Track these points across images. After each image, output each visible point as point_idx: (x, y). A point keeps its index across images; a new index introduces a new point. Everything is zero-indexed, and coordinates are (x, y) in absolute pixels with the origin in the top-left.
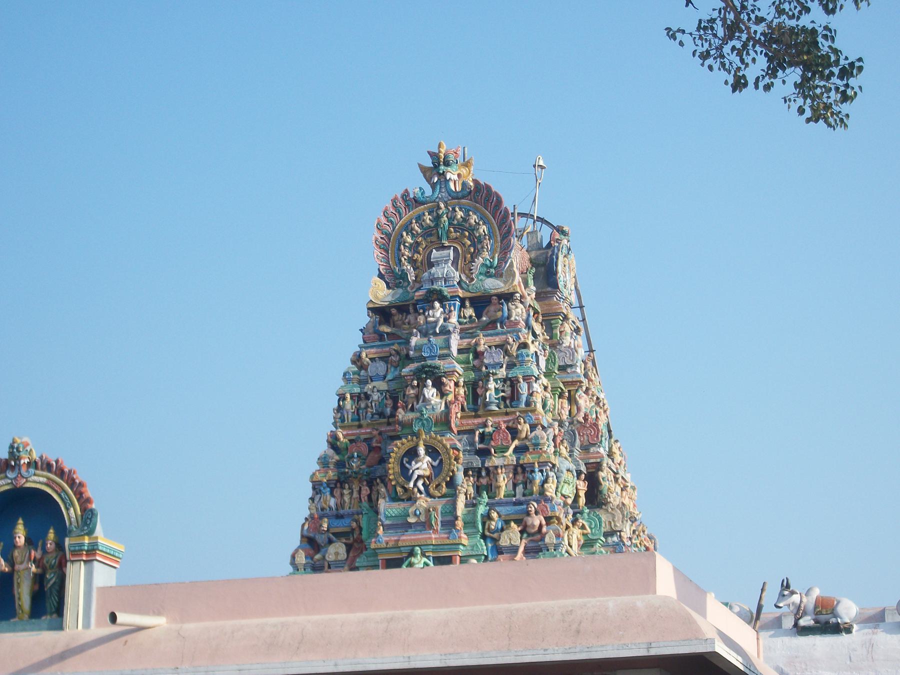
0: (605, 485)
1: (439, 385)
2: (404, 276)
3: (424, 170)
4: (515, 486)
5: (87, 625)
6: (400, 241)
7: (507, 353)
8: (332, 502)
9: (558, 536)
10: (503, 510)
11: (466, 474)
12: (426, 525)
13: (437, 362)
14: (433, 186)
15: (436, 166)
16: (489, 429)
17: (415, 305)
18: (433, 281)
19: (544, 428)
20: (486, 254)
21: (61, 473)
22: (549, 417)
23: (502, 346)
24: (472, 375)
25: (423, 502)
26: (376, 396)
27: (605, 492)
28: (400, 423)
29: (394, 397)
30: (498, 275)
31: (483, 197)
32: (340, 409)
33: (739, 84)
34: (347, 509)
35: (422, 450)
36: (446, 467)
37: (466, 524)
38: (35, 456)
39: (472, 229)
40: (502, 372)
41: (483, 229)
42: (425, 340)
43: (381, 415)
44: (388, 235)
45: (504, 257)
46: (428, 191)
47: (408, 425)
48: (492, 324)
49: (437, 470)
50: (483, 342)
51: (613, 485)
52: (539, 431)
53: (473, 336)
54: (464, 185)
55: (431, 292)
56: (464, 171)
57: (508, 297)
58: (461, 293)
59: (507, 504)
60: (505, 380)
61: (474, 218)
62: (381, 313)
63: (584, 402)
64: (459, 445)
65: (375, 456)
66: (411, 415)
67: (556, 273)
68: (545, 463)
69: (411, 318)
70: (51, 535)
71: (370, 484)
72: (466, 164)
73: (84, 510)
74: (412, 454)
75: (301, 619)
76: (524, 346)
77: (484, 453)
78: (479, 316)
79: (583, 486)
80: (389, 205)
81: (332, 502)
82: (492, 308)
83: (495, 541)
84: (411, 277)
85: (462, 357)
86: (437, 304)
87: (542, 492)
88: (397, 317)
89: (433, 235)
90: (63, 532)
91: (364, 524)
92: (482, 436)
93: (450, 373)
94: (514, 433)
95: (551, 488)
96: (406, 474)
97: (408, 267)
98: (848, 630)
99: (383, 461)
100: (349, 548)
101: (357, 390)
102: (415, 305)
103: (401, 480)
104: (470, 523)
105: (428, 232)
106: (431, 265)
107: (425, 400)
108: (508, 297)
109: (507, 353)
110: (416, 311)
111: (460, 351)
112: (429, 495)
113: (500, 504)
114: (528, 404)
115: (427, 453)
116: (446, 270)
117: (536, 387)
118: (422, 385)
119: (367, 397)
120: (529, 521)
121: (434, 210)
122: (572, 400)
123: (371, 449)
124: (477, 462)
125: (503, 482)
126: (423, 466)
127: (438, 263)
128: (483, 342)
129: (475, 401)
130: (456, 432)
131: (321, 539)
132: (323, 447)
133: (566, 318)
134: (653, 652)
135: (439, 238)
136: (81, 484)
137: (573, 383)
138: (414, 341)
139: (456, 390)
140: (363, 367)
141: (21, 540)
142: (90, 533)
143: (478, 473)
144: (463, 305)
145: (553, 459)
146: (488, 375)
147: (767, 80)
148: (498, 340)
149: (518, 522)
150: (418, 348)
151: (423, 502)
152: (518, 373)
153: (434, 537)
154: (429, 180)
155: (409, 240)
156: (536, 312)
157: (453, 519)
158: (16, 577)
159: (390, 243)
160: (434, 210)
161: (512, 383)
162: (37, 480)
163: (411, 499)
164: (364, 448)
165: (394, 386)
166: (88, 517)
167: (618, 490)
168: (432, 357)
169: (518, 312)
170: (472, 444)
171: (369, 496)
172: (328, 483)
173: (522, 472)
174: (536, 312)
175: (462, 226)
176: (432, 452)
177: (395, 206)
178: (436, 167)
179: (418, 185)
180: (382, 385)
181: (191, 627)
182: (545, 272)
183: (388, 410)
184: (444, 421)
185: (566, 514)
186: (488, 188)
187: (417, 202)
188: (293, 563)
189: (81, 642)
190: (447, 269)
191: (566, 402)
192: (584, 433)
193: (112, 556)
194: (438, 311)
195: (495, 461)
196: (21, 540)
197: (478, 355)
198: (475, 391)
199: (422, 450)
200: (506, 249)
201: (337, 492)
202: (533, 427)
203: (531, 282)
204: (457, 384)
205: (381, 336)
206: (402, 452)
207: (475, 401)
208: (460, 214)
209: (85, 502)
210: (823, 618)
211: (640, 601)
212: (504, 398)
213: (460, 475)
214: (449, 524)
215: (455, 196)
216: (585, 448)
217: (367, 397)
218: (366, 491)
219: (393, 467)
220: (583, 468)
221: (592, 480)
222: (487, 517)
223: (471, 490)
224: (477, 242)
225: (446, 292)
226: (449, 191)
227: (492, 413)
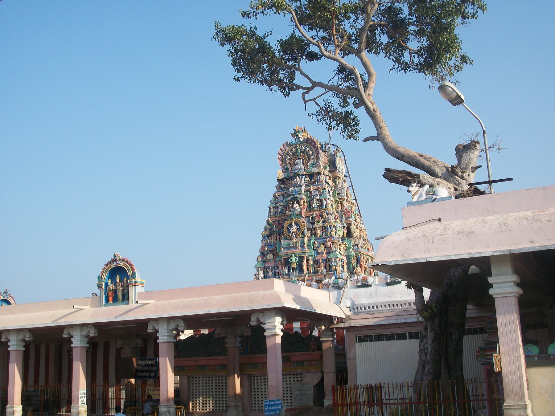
0: (352, 230)
1: (298, 203)
2: (287, 169)
4: (323, 233)
6: (286, 158)
7: (319, 191)
9: (335, 248)
10: (319, 241)
11: (308, 230)
12: (296, 247)
13: (298, 196)
14: (295, 139)
15: (295, 133)
16: (314, 216)
18: (296, 170)
19: (331, 214)
20: (312, 160)
21: (127, 262)
22: (334, 210)
23: (318, 189)
25: (294, 240)
26: (280, 207)
27: (353, 232)
28: (287, 216)
29: (286, 207)
30: (316, 167)
31: (310, 142)
32: (270, 212)
33: (330, 129)
35: (293, 224)
36: (301, 228)
37: (308, 246)
38: (121, 258)
39: (308, 153)
40: (318, 197)
41: (311, 152)
43: (282, 213)
45: (317, 161)
46: (294, 141)
48: (314, 183)
50: (312, 188)
51: (356, 230)
52: (330, 215)
53: (309, 186)
55: (295, 173)
56: (304, 134)
57: (319, 173)
58: (305, 173)
59: (320, 239)
60: (318, 200)
61: (308, 149)
62: (281, 181)
63: (345, 204)
64: (305, 221)
66: (290, 213)
67: (336, 164)
68: (331, 226)
69: (290, 182)
70: (125, 279)
71: (280, 235)
72: (305, 132)
74: (291, 225)
75: (185, 300)
76: (325, 189)
77: (313, 223)
78: (311, 180)
79: (345, 231)
80: (282, 146)
83: (317, 250)
84: (290, 169)
85: (306, 193)
86: (297, 177)
87: (331, 235)
88: (286, 182)
89: (296, 155)
91: (277, 247)
92: (312, 218)
93: (302, 199)
94: (322, 216)
95: (333, 233)
96: (289, 231)
97: (289, 166)
98: (371, 286)
99: (283, 227)
100: (274, 255)
101: (275, 206)
103: (288, 233)
104: (309, 246)
106: (296, 165)
108: (319, 173)
109: (319, 191)
111: (305, 191)
112: (297, 238)
113: (318, 239)
114: (326, 207)
115: (295, 224)
116: (300, 166)
117: (328, 201)
118: (293, 203)
120: (327, 244)
121: (296, 147)
122: (342, 204)
123: (279, 224)
124: (311, 226)
125: (319, 232)
126: (294, 229)
127: (297, 164)
128: (312, 188)
129: (310, 207)
130: (304, 217)
131: (265, 253)
132: (265, 224)
133: (340, 178)
134: (269, 307)
135: (298, 156)
137: (342, 199)
138: (291, 189)
140: (276, 198)
141: (118, 280)
142: (134, 278)
143: (311, 229)
144: (306, 177)
145: (334, 224)
147: (336, 127)
148: (316, 187)
149: (324, 244)
150: (292, 192)
152: (322, 197)
153: (298, 251)
155: (289, 157)
156: (330, 177)
157: (7, 340)
159: (283, 159)
160: (296, 147)
161: (321, 200)
162: (121, 264)
164: (277, 224)
166: (134, 274)
167: (358, 231)
168: (296, 194)
169: (322, 178)
170: (309, 221)
171: (279, 239)
172: (267, 235)
173: (324, 228)
174: (330, 177)
175: (304, 152)
176: (297, 224)
177: (283, 147)
178: (295, 134)
179: (291, 140)
180: (282, 204)
181: (159, 303)
182: (332, 164)
184: (300, 214)
185: (339, 241)
187: (290, 145)
188: (257, 261)
190: (301, 166)
191: (340, 205)
192: (346, 214)
193: (142, 284)
195: (316, 226)
196: (118, 280)
197: (310, 192)
198: (310, 203)
199: (293, 224)
200: (318, 158)
201: (270, 238)
202: (328, 214)
203: (328, 167)
204: (304, 202)
207: (310, 207)
208: (303, 148)
209: (133, 270)
210: (364, 283)
211: (268, 292)
212: (319, 206)
213: (306, 231)
214: (303, 246)
215: (302, 142)
216: (346, 219)
217: (278, 207)
218: (278, 237)
219: (285, 229)
220: (345, 226)
221: (348, 229)
222: (314, 243)
223: (309, 235)
224: (309, 156)
225: (300, 173)
226: (300, 141)
227: (315, 211)
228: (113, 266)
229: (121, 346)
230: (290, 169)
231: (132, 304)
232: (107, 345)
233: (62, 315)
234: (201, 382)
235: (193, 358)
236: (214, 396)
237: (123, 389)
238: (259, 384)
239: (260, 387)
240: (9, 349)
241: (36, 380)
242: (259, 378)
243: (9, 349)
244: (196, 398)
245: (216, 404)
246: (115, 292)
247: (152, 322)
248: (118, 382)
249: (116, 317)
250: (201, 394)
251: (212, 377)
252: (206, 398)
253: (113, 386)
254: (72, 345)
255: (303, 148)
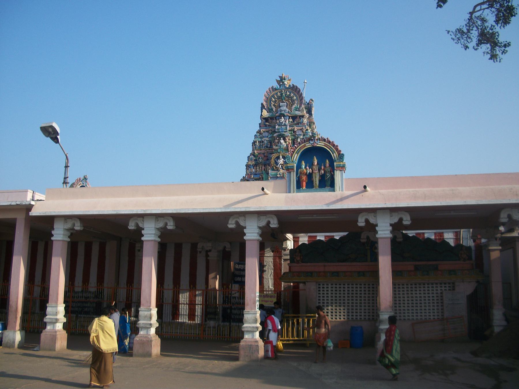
1: (284, 139)
2: (272, 109)
3: (277, 81)
5: (342, 190)
6: (271, 100)
8: (254, 170)
13: (283, 133)
14: (280, 85)
17: (276, 118)
20: (296, 105)
23: (301, 130)
24: (293, 137)
25: (282, 171)
26: (265, 142)
30: (299, 111)
31: (295, 89)
34: (258, 173)
35: (281, 157)
38: (320, 137)
39: (292, 98)
40: (302, 137)
41: (295, 98)
42: (280, 127)
43: (267, 147)
44: (268, 98)
46: (279, 87)
47: (277, 150)
49: (285, 162)
54: (289, 85)
55: (281, 114)
56: (289, 82)
57: (303, 116)
58: (289, 115)
61: (292, 95)
65: (266, 158)
66: (277, 147)
69: (274, 121)
72: (289, 80)
73: (339, 154)
74: (278, 158)
78: (294, 121)
81: (254, 170)
82: (297, 119)
84: (274, 110)
85: (290, 132)
88: (270, 121)
89: (281, 99)
90: (332, 162)
97: (273, 106)
102: (276, 118)
105: (279, 98)
106: (280, 107)
107: (281, 143)
108: (303, 116)
109: (302, 132)
110: (276, 119)
112: (283, 169)
116: (284, 108)
119: (263, 142)
121: (281, 92)
123: (265, 156)
126: (281, 161)
127: (282, 106)
135: (282, 100)
136: (337, 146)
138: (277, 127)
139: (289, 141)
144: (289, 118)
146: (298, 137)
148: (300, 128)
150: (278, 129)
151: (282, 171)
154: (279, 84)
158: (314, 175)
160: (281, 92)
162: (321, 144)
163: (278, 170)
164: (263, 156)
165: (270, 139)
175: (289, 97)
176: (284, 157)
177: (269, 90)
178: (281, 81)
180: (267, 139)
183: (269, 146)
186: (296, 86)
187: (276, 89)
189: (346, 195)
194: (283, 119)
197: (294, 132)
199: (281, 157)
205: (266, 125)
206: (276, 157)
208: (288, 93)
209: (339, 152)
218: (263, 167)
219: (273, 161)
224: (293, 102)
225: (285, 114)
226: (285, 87)
228: (308, 145)
229: (210, 248)
230: (274, 110)
231: (338, 193)
232: (178, 247)
233: (240, 199)
234: (330, 289)
235: (320, 264)
236: (346, 304)
237: (199, 295)
238: (401, 293)
239: (401, 296)
240: (143, 239)
241: (86, 280)
242: (401, 286)
243: (143, 239)
244: (328, 306)
245: (348, 312)
246: (310, 176)
247: (364, 213)
248: (193, 285)
249: (328, 204)
250: (330, 301)
251: (344, 285)
252: (336, 306)
253: (185, 291)
254: (245, 238)
255: (288, 93)
